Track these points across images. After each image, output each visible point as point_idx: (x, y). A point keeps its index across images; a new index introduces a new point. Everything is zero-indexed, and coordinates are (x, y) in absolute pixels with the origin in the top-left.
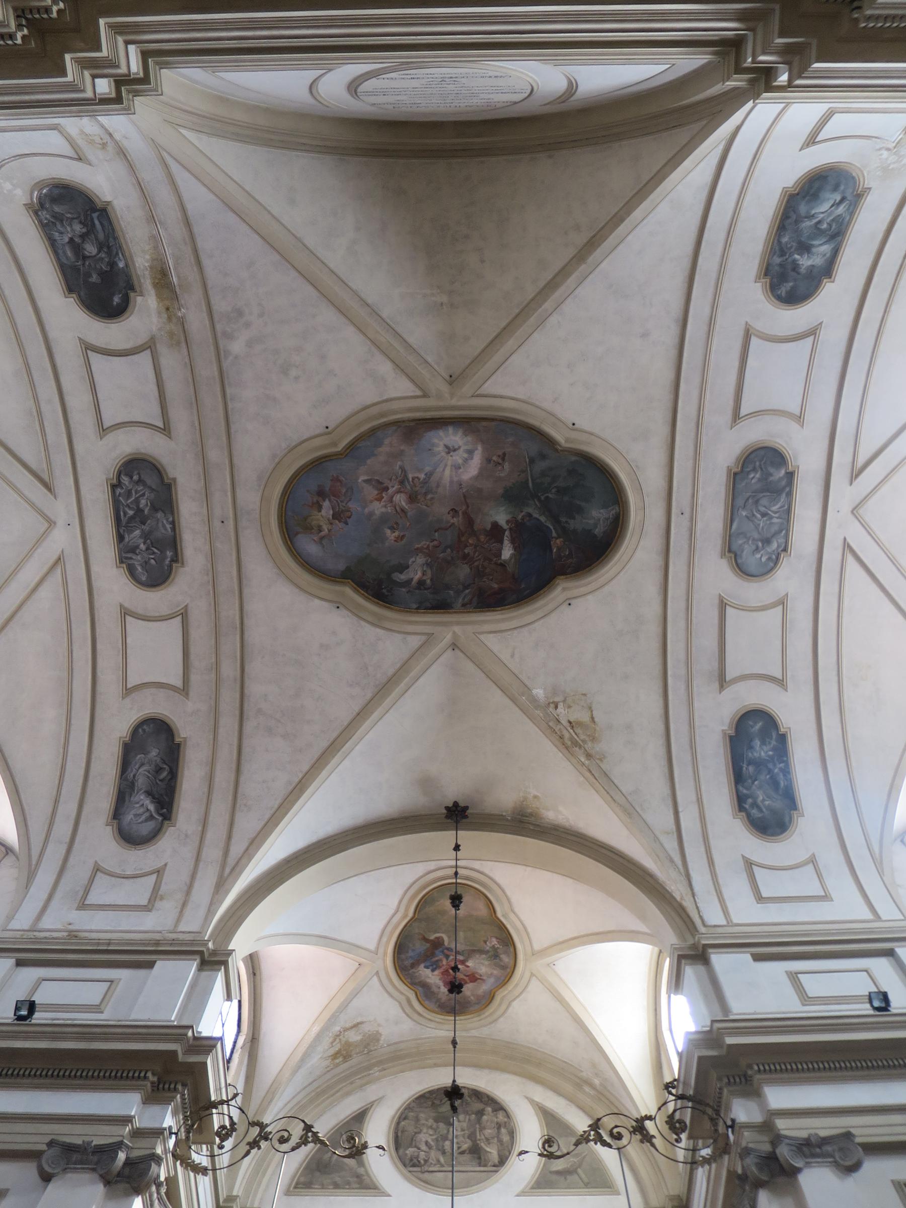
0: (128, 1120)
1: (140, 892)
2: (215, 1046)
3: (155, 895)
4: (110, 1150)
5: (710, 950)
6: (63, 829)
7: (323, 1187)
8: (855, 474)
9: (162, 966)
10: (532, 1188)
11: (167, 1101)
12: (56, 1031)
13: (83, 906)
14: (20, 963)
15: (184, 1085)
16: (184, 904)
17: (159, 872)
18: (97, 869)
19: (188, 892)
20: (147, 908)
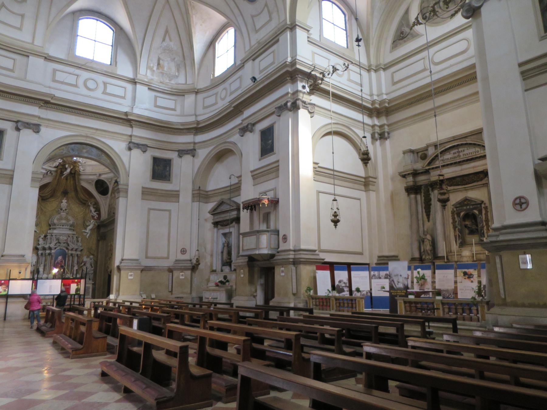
0: (288, 93)
1: (265, 17)
2: (296, 62)
3: (270, 14)
4: (286, 104)
5: (297, 27)
6: (236, 11)
7: (115, 204)
8: (167, 32)
9: (281, 38)
10: (392, 48)
11: (296, 81)
12: (262, 81)
13: (257, 31)
14: (254, 60)
15: (298, 75)
16: (278, 11)
17: (266, 5)
18: (253, 17)
19: (277, 6)
20: (271, 20)
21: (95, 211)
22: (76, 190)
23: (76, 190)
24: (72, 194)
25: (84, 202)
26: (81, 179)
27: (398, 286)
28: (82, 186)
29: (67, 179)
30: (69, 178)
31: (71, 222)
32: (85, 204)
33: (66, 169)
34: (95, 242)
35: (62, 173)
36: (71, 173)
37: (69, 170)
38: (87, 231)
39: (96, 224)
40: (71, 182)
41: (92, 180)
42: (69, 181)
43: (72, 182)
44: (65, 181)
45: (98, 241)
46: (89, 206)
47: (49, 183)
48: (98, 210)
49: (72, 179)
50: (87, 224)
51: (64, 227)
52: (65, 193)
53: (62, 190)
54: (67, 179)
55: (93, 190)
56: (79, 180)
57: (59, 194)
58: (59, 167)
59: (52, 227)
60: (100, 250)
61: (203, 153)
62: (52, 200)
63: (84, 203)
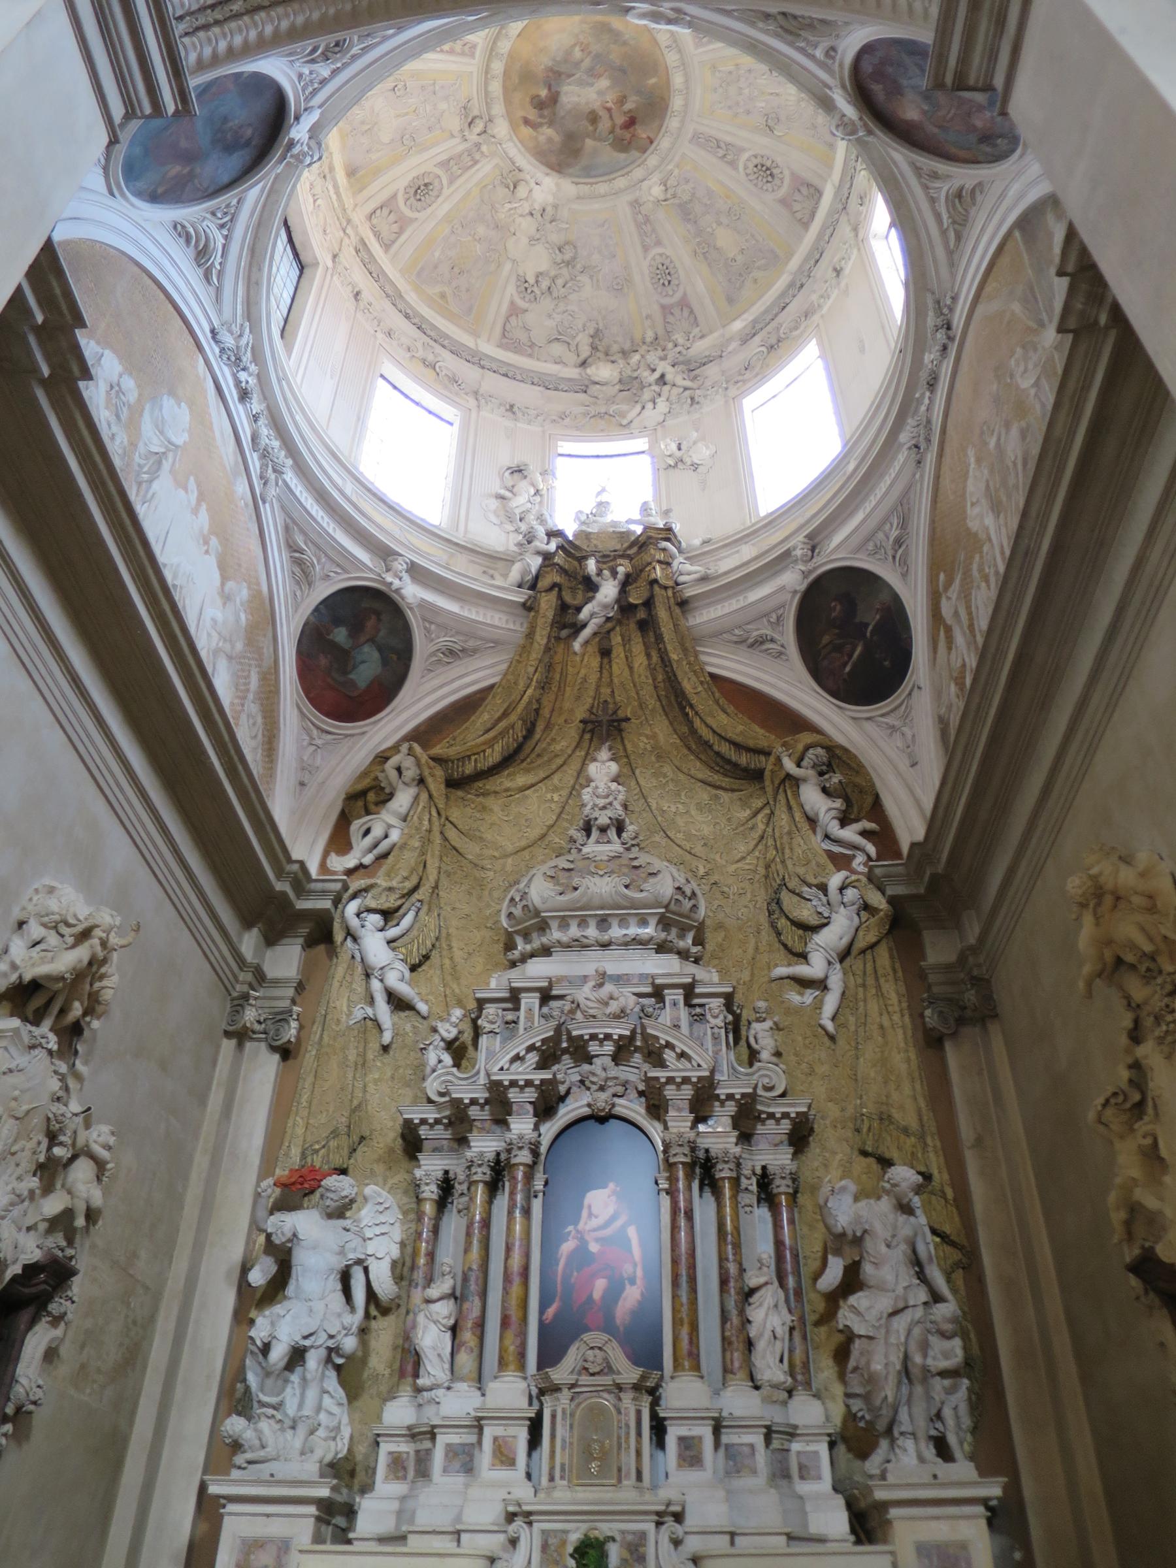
21: (844, 822)
22: (676, 700)
23: (676, 700)
24: (654, 731)
25: (743, 759)
26: (697, 640)
27: (960, 1353)
28: (713, 676)
29: (606, 653)
30: (616, 639)
31: (664, 886)
32: (755, 776)
33: (590, 586)
34: (903, 1056)
35: (566, 621)
36: (625, 608)
37: (608, 591)
38: (815, 967)
39: (877, 900)
40: (633, 661)
41: (770, 614)
42: (618, 652)
43: (640, 661)
44: (595, 662)
45: (932, 1042)
46: (794, 782)
47: (492, 687)
48: (860, 800)
49: (637, 647)
50: (805, 913)
51: (616, 932)
52: (604, 727)
53: (581, 713)
54: (606, 653)
55: (790, 684)
56: (689, 643)
57: (565, 740)
58: (544, 583)
59: (521, 946)
60: (966, 1130)
61: (1149, 1022)
62: (521, 780)
63: (743, 772)
